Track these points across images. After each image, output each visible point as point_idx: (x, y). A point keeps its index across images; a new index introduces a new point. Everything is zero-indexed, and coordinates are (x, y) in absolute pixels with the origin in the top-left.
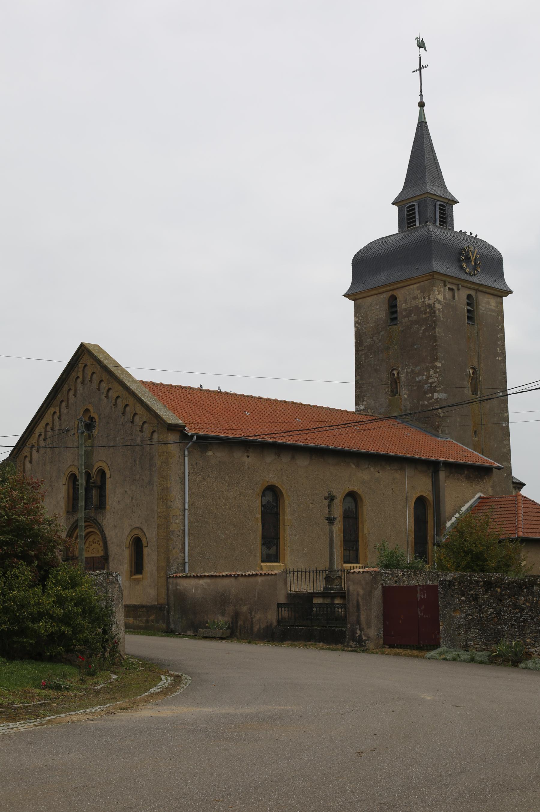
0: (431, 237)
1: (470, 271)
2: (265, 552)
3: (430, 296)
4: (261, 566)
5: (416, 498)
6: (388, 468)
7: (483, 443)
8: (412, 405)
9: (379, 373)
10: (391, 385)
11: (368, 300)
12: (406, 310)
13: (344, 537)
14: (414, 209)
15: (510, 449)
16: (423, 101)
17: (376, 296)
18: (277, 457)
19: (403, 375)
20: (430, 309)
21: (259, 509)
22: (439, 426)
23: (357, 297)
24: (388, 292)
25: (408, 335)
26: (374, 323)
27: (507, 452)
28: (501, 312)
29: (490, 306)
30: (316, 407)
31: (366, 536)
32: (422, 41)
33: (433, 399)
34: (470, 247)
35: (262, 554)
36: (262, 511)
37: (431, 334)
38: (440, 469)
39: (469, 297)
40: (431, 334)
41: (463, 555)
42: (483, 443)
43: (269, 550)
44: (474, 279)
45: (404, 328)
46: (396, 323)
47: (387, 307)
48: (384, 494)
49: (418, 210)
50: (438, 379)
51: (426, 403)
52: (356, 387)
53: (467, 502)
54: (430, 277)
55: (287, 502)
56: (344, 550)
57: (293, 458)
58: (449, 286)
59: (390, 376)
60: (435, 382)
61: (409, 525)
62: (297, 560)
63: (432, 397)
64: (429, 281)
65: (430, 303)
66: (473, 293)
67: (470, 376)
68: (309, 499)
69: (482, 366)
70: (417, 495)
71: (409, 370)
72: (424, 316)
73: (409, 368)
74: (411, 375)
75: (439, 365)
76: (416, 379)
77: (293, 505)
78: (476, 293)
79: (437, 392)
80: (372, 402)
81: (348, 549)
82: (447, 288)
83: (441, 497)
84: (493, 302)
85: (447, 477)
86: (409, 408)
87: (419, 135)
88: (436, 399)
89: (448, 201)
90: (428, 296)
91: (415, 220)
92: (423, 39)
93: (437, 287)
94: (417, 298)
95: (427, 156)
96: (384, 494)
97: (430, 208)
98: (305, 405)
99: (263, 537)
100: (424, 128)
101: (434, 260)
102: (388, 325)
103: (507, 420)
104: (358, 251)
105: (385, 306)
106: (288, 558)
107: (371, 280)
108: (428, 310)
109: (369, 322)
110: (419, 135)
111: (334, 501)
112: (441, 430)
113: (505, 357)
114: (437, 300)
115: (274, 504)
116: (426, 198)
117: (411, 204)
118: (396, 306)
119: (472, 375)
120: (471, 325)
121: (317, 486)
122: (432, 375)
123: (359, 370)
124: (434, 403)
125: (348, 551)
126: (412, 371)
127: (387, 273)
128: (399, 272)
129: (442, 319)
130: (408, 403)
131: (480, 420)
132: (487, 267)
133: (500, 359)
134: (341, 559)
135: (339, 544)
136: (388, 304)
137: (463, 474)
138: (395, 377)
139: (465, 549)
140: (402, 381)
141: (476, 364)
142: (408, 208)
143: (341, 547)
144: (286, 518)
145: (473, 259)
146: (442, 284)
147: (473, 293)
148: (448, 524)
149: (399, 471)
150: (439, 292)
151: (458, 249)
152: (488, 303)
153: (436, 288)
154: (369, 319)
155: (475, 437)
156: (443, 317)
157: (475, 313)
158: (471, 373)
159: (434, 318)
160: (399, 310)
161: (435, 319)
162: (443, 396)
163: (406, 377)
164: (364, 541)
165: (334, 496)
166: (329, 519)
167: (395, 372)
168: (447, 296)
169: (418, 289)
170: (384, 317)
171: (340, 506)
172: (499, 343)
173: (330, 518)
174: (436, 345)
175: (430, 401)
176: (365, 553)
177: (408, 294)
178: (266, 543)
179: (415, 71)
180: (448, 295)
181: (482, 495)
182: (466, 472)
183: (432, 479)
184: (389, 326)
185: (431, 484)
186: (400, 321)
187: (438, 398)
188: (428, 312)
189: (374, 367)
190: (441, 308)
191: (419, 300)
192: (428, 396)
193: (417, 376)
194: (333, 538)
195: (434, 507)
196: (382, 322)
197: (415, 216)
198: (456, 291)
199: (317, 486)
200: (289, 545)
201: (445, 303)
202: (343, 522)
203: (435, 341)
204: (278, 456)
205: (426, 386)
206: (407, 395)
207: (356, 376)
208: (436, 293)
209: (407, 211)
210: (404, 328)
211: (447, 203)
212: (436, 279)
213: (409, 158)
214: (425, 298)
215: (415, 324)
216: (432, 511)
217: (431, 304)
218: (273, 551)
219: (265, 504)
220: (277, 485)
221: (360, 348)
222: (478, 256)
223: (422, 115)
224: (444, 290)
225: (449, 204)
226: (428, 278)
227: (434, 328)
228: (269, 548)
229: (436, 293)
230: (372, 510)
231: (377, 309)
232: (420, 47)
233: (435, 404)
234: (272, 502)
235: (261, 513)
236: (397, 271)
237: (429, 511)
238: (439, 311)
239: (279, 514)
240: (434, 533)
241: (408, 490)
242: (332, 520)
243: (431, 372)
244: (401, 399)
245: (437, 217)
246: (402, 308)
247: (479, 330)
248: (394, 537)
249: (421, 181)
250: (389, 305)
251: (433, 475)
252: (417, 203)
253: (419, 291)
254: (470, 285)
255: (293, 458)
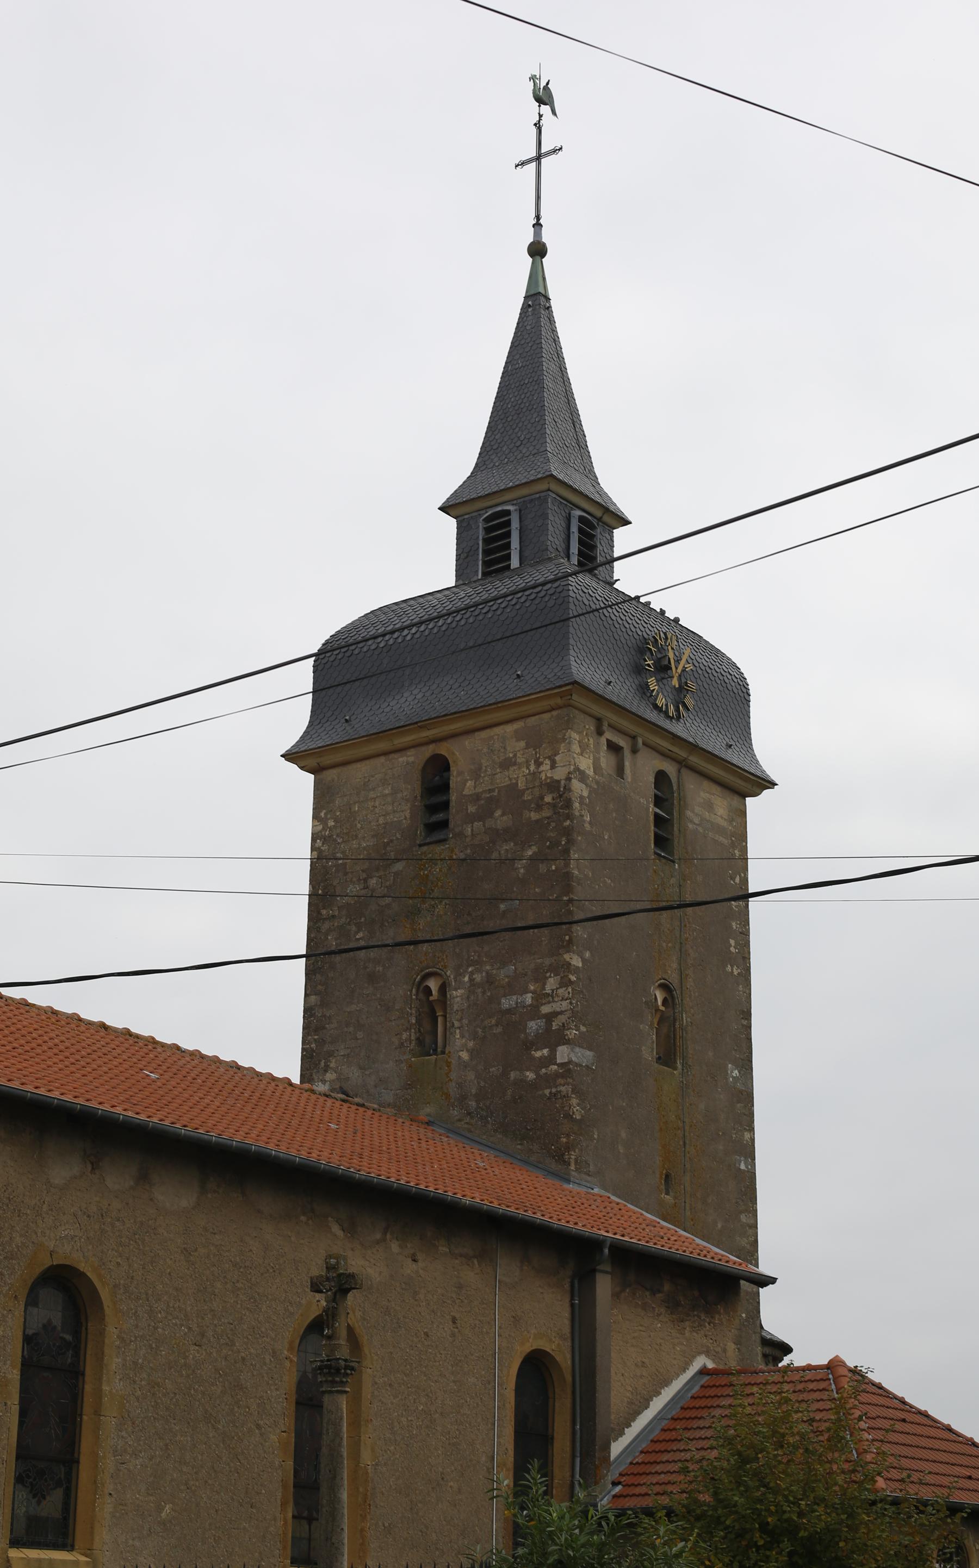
0: (566, 588)
1: (667, 705)
2: (24, 1509)
3: (557, 758)
4: (8, 1560)
5: (524, 1355)
6: (443, 1249)
7: (688, 1213)
8: (482, 1084)
9: (382, 984)
10: (419, 1021)
11: (359, 772)
12: (476, 798)
13: (296, 1472)
14: (508, 523)
15: (756, 1241)
16: (544, 240)
17: (382, 759)
18: (90, 1169)
19: (460, 992)
20: (555, 795)
21: (15, 1348)
22: (568, 1148)
23: (327, 760)
24: (423, 748)
25: (481, 874)
26: (373, 836)
27: (748, 1247)
28: (740, 837)
29: (713, 816)
30: (196, 1055)
31: (367, 1473)
32: (546, 88)
33: (555, 1064)
34: (669, 637)
35: (13, 1514)
36: (23, 1356)
37: (554, 868)
38: (598, 1267)
39: (661, 778)
40: (554, 868)
41: (761, 1543)
42: (688, 1213)
43: (39, 1503)
44: (678, 729)
45: (469, 851)
46: (442, 837)
47: (418, 792)
48: (426, 1334)
49: (518, 526)
50: (571, 1003)
51: (530, 1075)
52: (305, 1028)
53: (667, 1383)
54: (559, 701)
55: (112, 1332)
56: (294, 1517)
57: (143, 1178)
58: (609, 735)
59: (417, 994)
60: (561, 1013)
61: (499, 1443)
62: (137, 1543)
63: (551, 1059)
64: (555, 713)
65: (556, 778)
66: (670, 768)
67: (657, 1010)
68: (190, 1329)
69: (690, 983)
70: (528, 1348)
71: (478, 978)
72: (534, 816)
73: (479, 971)
74: (484, 993)
75: (577, 962)
76: (499, 1003)
77: (132, 1346)
78: (679, 771)
79: (567, 1042)
80: (354, 1074)
81: (305, 1514)
82: (603, 740)
83: (598, 1359)
84: (722, 805)
85: (616, 1296)
86: (474, 1091)
87: (528, 328)
88: (561, 1065)
89: (601, 518)
90: (549, 758)
91: (509, 555)
92: (548, 83)
93: (580, 733)
94: (515, 764)
95: (548, 382)
96: (426, 1334)
97: (555, 523)
98: (163, 1045)
99: (23, 1454)
100: (543, 312)
101: (572, 652)
102: (418, 842)
103: (749, 1152)
104: (333, 633)
105: (410, 789)
106: (104, 1536)
107: (372, 712)
108: (548, 799)
109: (356, 836)
110: (528, 328)
111: (350, 1296)
112: (576, 1160)
113: (748, 970)
114: (577, 769)
115: (68, 1337)
116: (542, 494)
117: (499, 508)
118: (445, 787)
119: (662, 1008)
120: (664, 861)
121: (219, 1285)
122: (553, 991)
123: (318, 977)
124: (557, 1075)
125: (305, 1523)
126: (490, 981)
127: (423, 690)
128: (461, 688)
129: (587, 827)
130: (471, 1076)
131: (681, 1143)
132: (710, 705)
133: (736, 973)
134: (285, 1548)
135: (279, 1495)
136: (419, 783)
137: (659, 1291)
138: (431, 998)
139: (769, 1520)
140: (456, 1008)
141: (674, 979)
142: (487, 520)
143: (284, 1504)
144: (106, 1388)
145: (676, 671)
146: (591, 726)
147: (670, 768)
148: (616, 1448)
149: (476, 1262)
150: (583, 748)
151: (637, 637)
152: (710, 806)
153: (575, 736)
154: (359, 826)
155: (667, 1194)
156: (590, 823)
157: (675, 829)
158: (660, 1002)
159: (565, 821)
160: (453, 797)
161: (568, 826)
162: (582, 1056)
163: (468, 998)
164: (361, 1490)
165: (352, 1276)
166: (329, 1367)
167: (433, 984)
168: (603, 765)
169: (518, 736)
170: (406, 818)
171: (287, 1364)
172: (734, 924)
173: (333, 1363)
174: (571, 901)
175: (544, 1070)
176: (362, 1530)
177: (485, 750)
178: (28, 1477)
179: (523, 164)
180: (607, 761)
181: (710, 1365)
182: (667, 1287)
183: (572, 1298)
184: (420, 845)
185: (567, 1314)
186: (457, 830)
187: (570, 1062)
188: (548, 803)
189: (365, 968)
190: (585, 794)
191: (519, 768)
192: (538, 1054)
193: (505, 996)
194: (340, 1445)
195: (574, 1393)
196: (398, 836)
197: (510, 542)
198: (627, 753)
199: (219, 1285)
200: (110, 1487)
201: (597, 783)
202: (297, 1419)
203: (568, 889)
204: (92, 1164)
205: (533, 1026)
206: (468, 1050)
207: (306, 995)
208: (576, 748)
209: (484, 528)
210: (469, 851)
211: (599, 519)
212: (576, 708)
213: (496, 390)
214: (538, 764)
215: (506, 841)
216: (568, 1402)
217: (558, 782)
218: (51, 1506)
219: (34, 1334)
220: (82, 1267)
221: (324, 912)
222: (690, 667)
223: (537, 278)
224: (597, 744)
225: (605, 523)
226: (552, 702)
227: (566, 851)
228: (38, 1494)
229: (576, 748)
230: (390, 1385)
231: (386, 795)
232: (540, 101)
233: (560, 1081)
234: (59, 1328)
235: (19, 1366)
236: (457, 685)
237: (557, 1404)
238: (581, 803)
239: (83, 1374)
240: (573, 1476)
241: (500, 1328)
242: (338, 1370)
243: (552, 983)
244: (449, 1064)
245: (571, 551)
246: (466, 792)
247: (684, 880)
248: (452, 1484)
249: (531, 448)
250: (423, 783)
251: (576, 1285)
252: (517, 507)
253: (522, 744)
254: (665, 744)
255: (143, 1178)
